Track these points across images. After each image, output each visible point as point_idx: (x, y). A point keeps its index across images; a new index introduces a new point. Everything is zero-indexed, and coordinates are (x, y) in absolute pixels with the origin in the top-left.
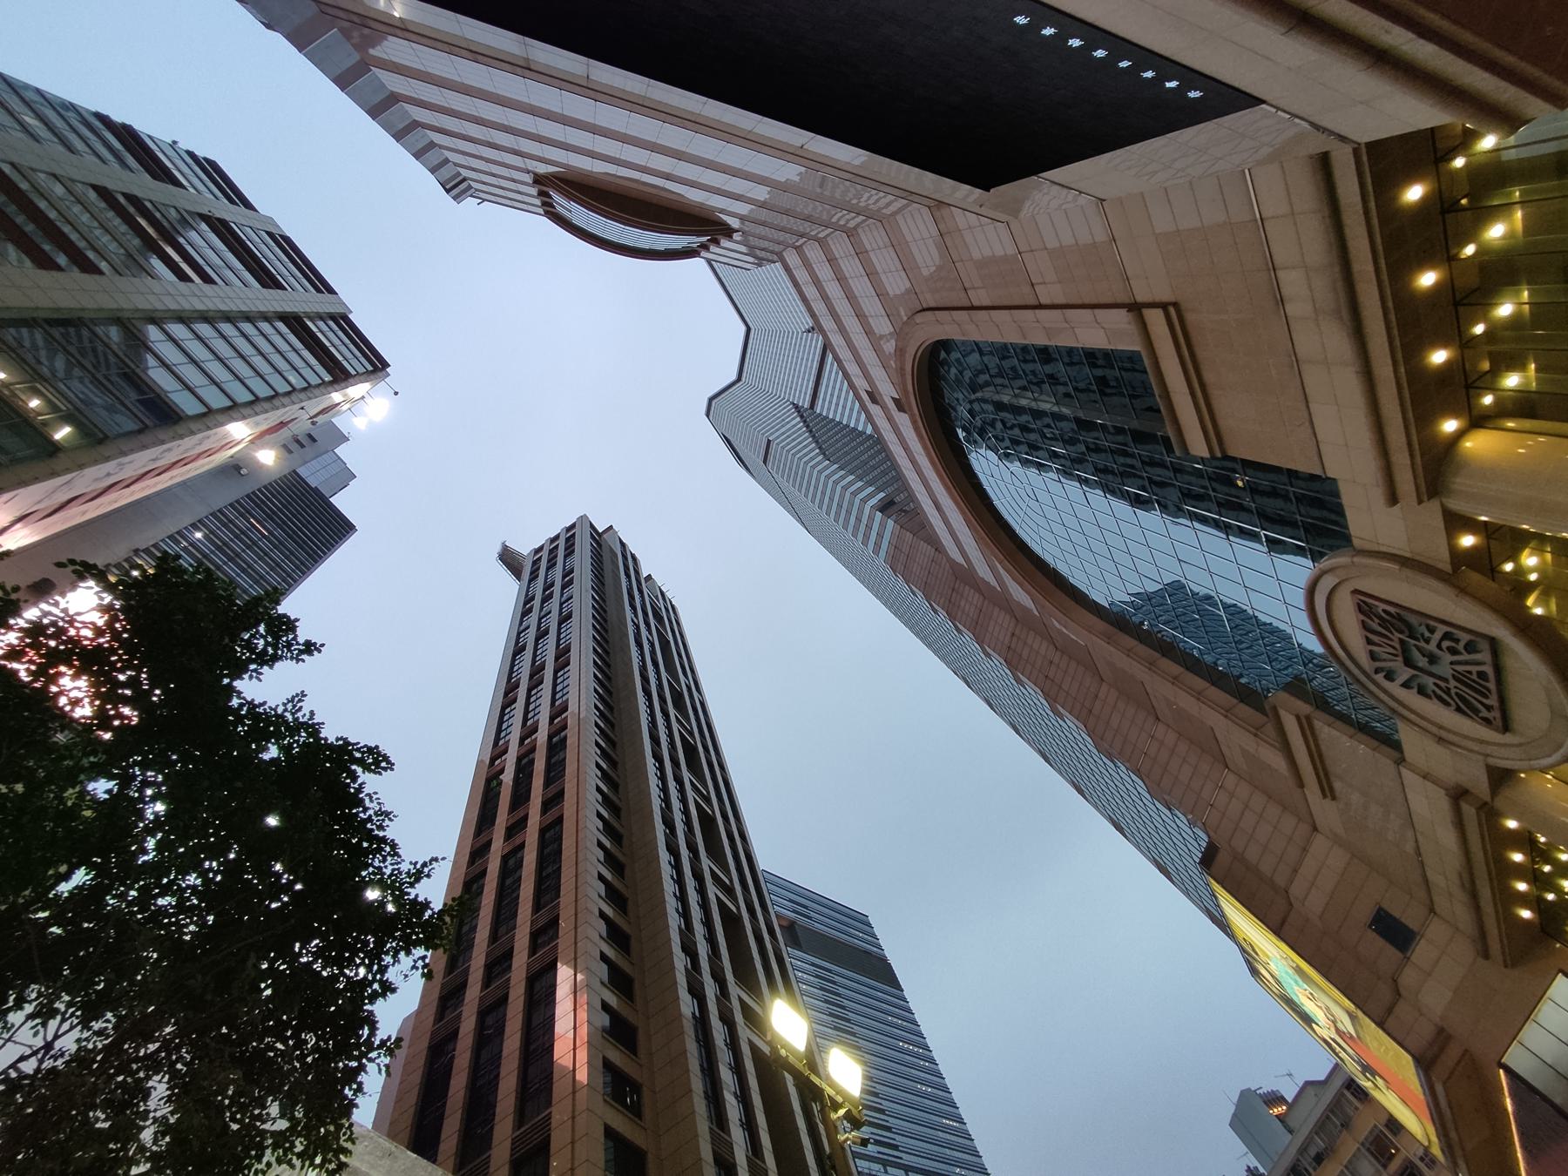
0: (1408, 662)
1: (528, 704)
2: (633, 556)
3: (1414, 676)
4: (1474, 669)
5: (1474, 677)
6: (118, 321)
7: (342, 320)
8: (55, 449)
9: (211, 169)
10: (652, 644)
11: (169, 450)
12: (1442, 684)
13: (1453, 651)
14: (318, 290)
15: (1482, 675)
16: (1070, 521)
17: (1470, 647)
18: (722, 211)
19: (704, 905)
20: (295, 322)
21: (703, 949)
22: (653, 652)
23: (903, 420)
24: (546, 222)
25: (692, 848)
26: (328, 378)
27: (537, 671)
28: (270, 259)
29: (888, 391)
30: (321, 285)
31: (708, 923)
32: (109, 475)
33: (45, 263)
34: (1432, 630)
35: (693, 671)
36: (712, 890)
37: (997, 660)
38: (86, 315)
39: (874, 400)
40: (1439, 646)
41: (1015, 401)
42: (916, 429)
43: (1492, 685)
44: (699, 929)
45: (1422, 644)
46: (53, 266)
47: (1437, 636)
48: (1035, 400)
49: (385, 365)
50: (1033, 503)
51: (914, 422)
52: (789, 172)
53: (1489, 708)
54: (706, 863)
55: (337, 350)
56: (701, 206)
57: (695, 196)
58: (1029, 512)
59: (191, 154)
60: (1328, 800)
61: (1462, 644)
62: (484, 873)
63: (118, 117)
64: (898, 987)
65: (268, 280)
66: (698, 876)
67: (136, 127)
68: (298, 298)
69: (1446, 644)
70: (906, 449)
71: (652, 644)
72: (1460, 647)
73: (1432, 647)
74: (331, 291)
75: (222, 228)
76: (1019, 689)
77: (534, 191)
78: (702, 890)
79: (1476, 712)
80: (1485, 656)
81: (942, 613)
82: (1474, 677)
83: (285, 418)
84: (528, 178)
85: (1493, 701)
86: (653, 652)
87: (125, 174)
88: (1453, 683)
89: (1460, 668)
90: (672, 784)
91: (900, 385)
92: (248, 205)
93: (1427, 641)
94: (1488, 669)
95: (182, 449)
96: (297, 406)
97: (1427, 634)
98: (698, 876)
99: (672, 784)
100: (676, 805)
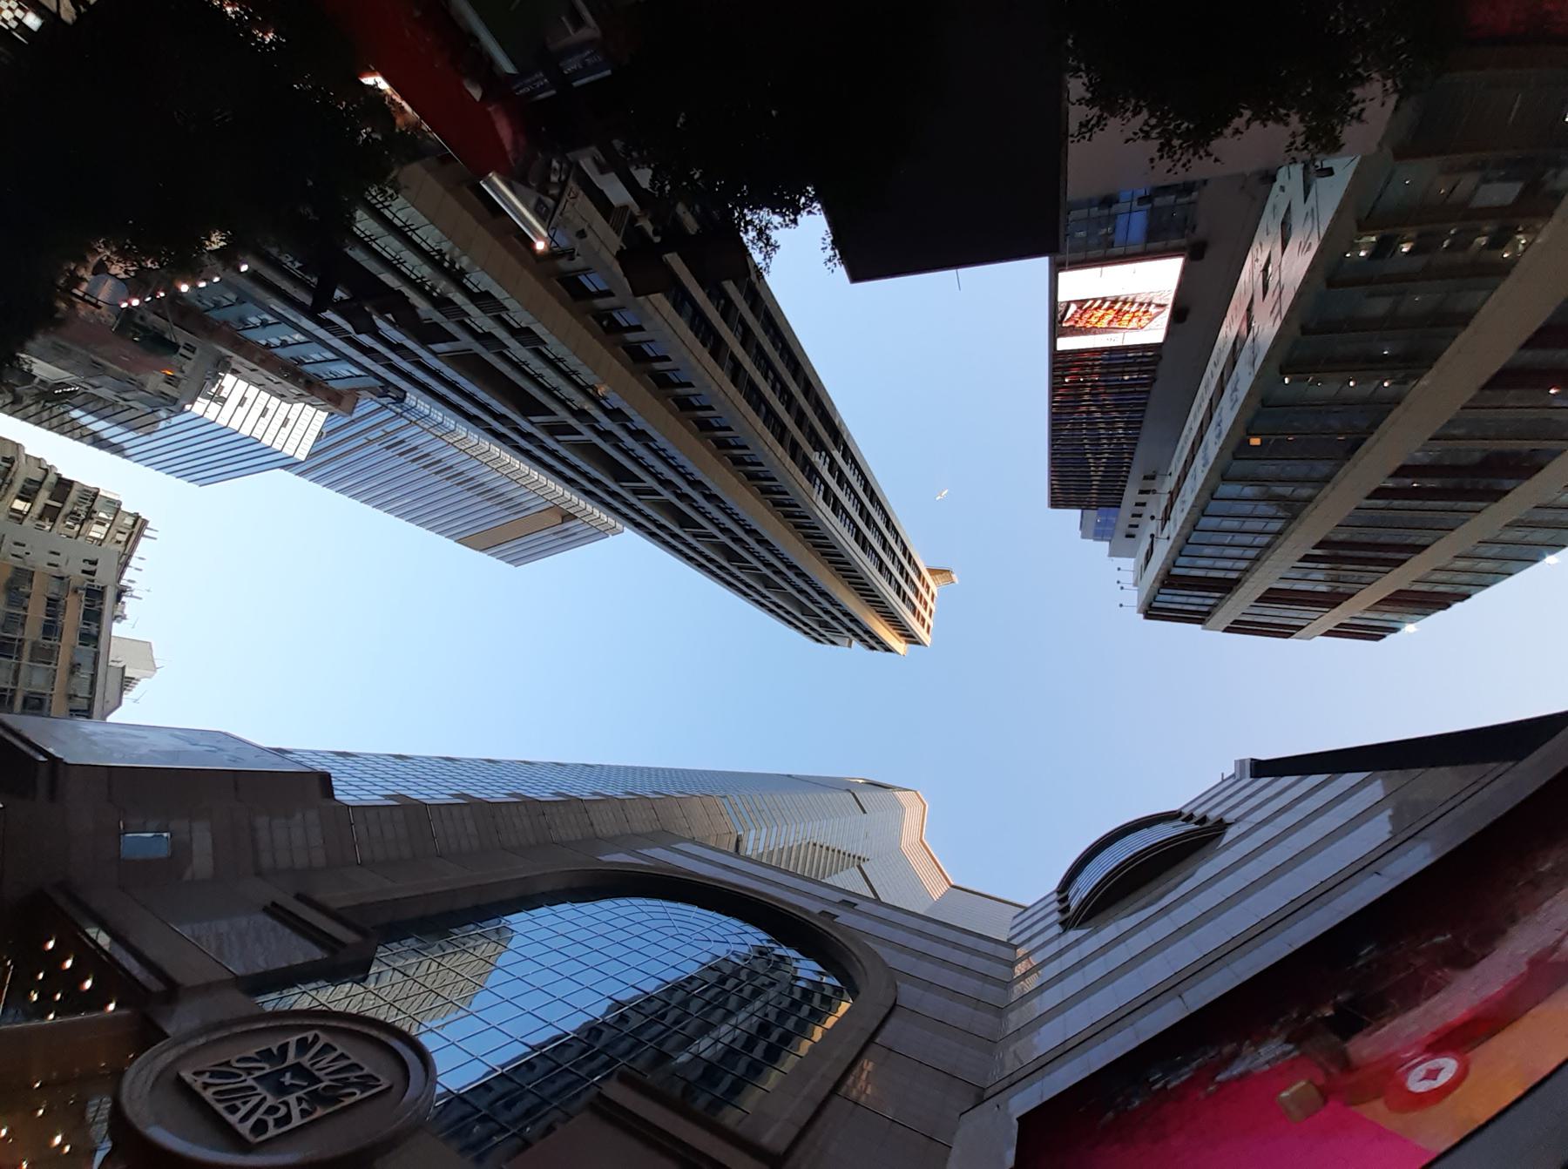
0: (297, 1069)
1: (857, 496)
2: (873, 648)
3: (284, 1060)
4: (244, 1110)
5: (238, 1103)
6: (1327, 479)
7: (1199, 617)
8: (1283, 373)
9: (1374, 633)
10: (814, 602)
11: (1219, 436)
12: (257, 1074)
13: (272, 1110)
14: (1236, 622)
15: (233, 1110)
16: (617, 951)
17: (260, 1127)
18: (1085, 937)
19: (646, 468)
20: (1227, 587)
21: (629, 442)
22: (808, 596)
23: (816, 908)
24: (1175, 807)
25: (683, 497)
26: (1176, 571)
27: (869, 520)
28: (1277, 615)
29: (845, 918)
30: (1237, 627)
31: (636, 460)
32: (1235, 390)
33: (1403, 471)
34: (304, 1113)
35: (771, 611)
36: (650, 482)
37: (587, 796)
38: (1348, 465)
39: (844, 902)
40: (286, 1104)
41: (763, 998)
42: (801, 908)
43: (220, 1107)
44: (640, 450)
45: (300, 1093)
46: (1394, 475)
47: (295, 1112)
48: (736, 1027)
49: (1148, 616)
50: (672, 932)
51: (807, 912)
52: (1047, 1039)
53: (206, 1086)
54: (667, 495)
55: (1181, 595)
56: (1106, 923)
57: (1109, 932)
58: (669, 923)
59: (1395, 630)
60: (268, 904)
61: (271, 1124)
62: (795, 378)
63: (1457, 607)
64: (458, 541)
65: (1272, 597)
66: (666, 483)
67: (1441, 613)
68: (1240, 604)
69: (283, 1111)
70: (788, 888)
71: (814, 602)
72: (270, 1120)
73: (292, 1099)
74: (1228, 630)
75: (1331, 600)
76: (552, 789)
77: (1213, 815)
78: (655, 475)
79: (213, 1075)
80: (245, 1129)
81: (651, 796)
82: (238, 1103)
83: (1170, 524)
84: (1228, 818)
85: (208, 1095)
86: (808, 596)
87: (1419, 574)
88: (250, 1082)
89: (255, 1100)
90: (729, 524)
91: (837, 927)
92: (1329, 633)
93: (299, 1100)
94: (233, 1119)
95: (1211, 445)
96: (1173, 536)
97: (304, 1105)
98: (666, 483)
99: (729, 524)
100: (716, 513)
